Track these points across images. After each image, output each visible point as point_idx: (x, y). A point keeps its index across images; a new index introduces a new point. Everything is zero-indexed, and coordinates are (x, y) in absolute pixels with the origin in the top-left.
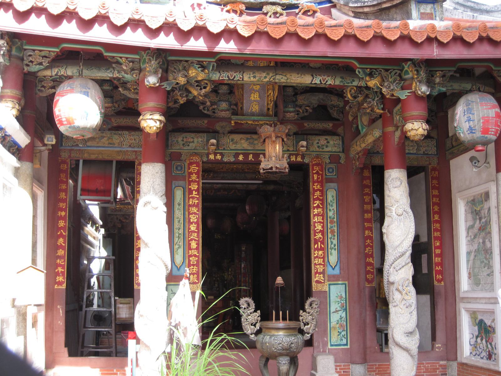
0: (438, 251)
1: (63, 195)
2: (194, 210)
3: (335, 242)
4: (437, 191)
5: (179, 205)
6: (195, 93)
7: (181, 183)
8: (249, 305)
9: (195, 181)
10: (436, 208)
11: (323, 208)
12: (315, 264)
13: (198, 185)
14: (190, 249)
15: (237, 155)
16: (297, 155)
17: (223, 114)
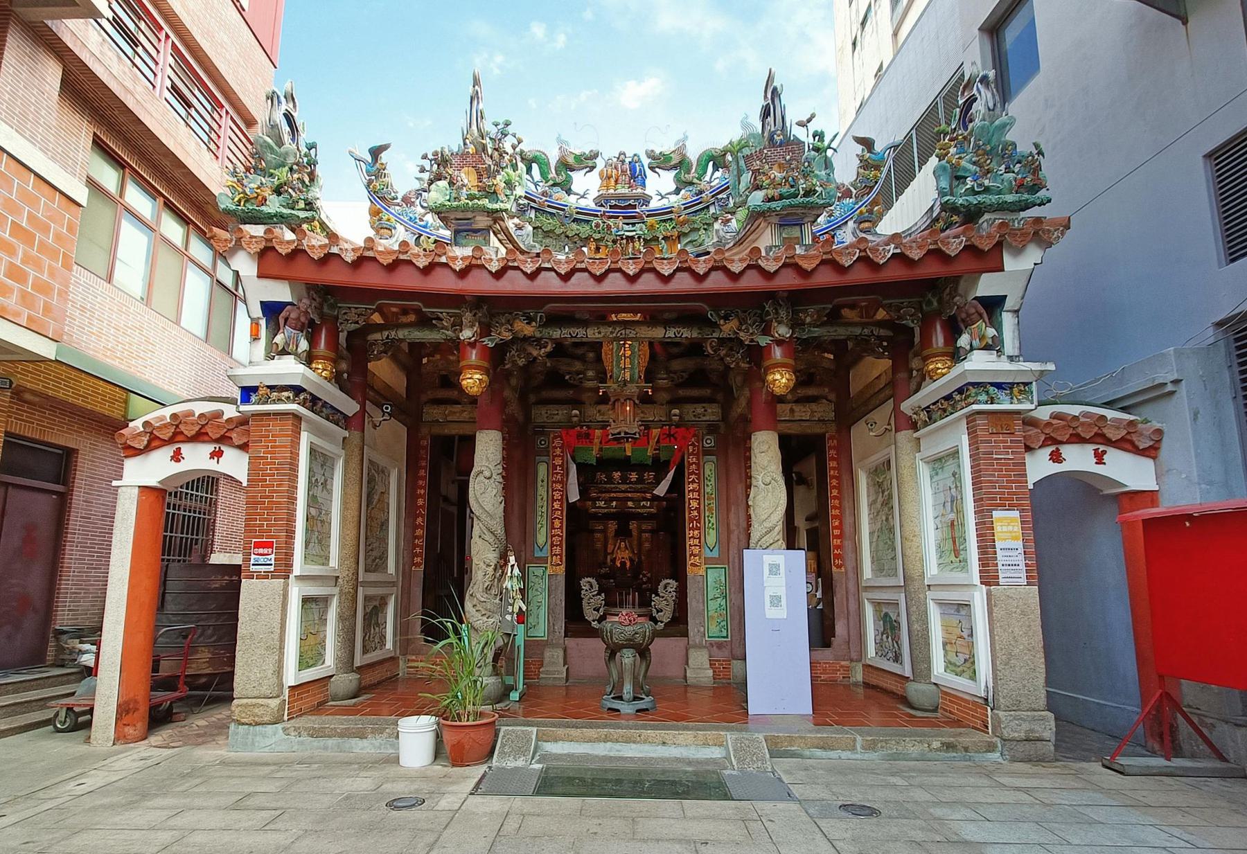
0: (837, 532)
3: (713, 520)
4: (835, 463)
5: (543, 481)
8: (591, 586)
12: (690, 545)
17: (590, 384)
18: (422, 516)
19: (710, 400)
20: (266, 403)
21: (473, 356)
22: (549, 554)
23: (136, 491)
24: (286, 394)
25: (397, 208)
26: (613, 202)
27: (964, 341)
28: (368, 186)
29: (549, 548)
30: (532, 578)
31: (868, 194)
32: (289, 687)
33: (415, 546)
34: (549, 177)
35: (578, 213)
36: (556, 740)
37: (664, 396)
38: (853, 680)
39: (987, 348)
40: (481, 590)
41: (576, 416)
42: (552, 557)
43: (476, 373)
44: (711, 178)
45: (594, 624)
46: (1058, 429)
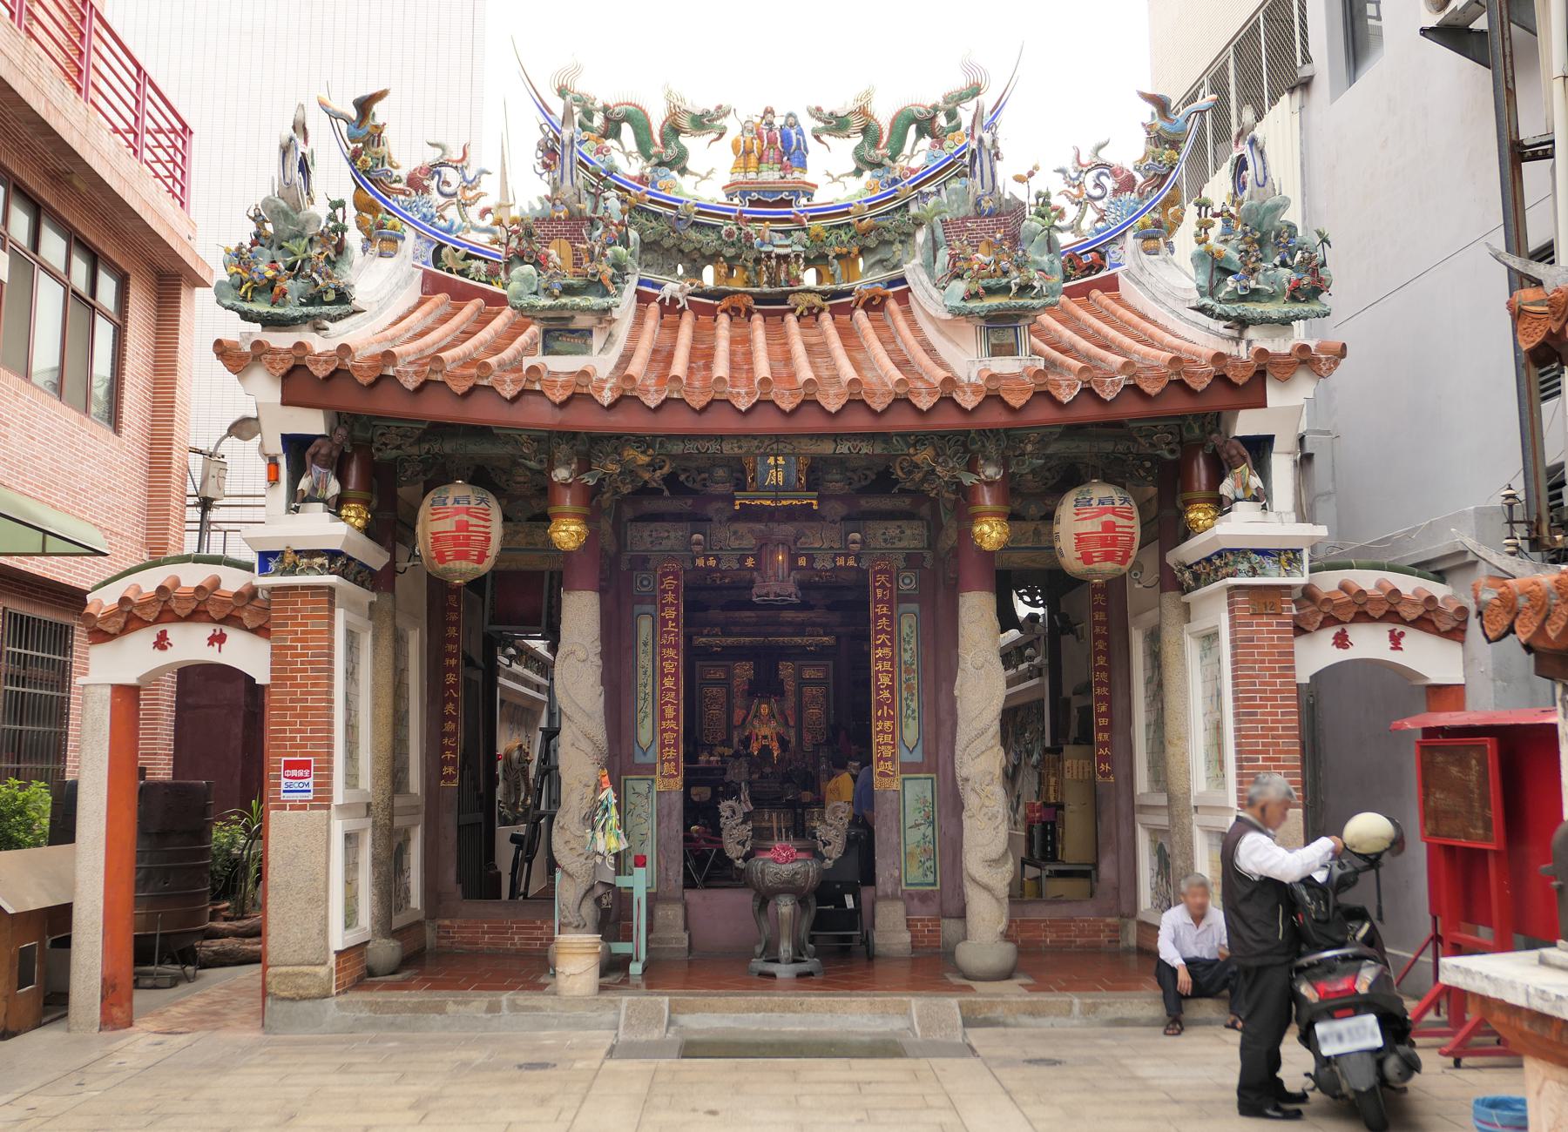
0: (1103, 722)
1: (452, 632)
2: (671, 652)
3: (914, 705)
5: (645, 644)
6: (647, 476)
7: (649, 608)
8: (734, 812)
9: (672, 604)
10: (1101, 645)
11: (892, 646)
13: (677, 610)
14: (663, 718)
15: (742, 560)
16: (847, 556)
17: (720, 489)
18: (455, 701)
19: (908, 516)
20: (292, 572)
21: (567, 502)
22: (658, 760)
23: (108, 691)
24: (319, 560)
25: (401, 197)
26: (755, 196)
27: (1227, 488)
28: (354, 158)
29: (658, 750)
30: (631, 798)
31: (1159, 187)
32: (336, 952)
33: (444, 749)
34: (652, 152)
35: (699, 213)
36: (693, 1011)
37: (839, 509)
38: (1122, 944)
39: (1255, 499)
40: (576, 820)
41: (698, 543)
42: (662, 764)
43: (573, 524)
44: (913, 149)
45: (739, 863)
46: (1340, 605)
